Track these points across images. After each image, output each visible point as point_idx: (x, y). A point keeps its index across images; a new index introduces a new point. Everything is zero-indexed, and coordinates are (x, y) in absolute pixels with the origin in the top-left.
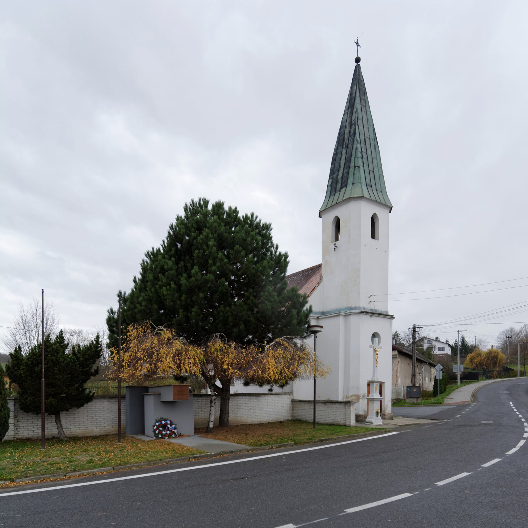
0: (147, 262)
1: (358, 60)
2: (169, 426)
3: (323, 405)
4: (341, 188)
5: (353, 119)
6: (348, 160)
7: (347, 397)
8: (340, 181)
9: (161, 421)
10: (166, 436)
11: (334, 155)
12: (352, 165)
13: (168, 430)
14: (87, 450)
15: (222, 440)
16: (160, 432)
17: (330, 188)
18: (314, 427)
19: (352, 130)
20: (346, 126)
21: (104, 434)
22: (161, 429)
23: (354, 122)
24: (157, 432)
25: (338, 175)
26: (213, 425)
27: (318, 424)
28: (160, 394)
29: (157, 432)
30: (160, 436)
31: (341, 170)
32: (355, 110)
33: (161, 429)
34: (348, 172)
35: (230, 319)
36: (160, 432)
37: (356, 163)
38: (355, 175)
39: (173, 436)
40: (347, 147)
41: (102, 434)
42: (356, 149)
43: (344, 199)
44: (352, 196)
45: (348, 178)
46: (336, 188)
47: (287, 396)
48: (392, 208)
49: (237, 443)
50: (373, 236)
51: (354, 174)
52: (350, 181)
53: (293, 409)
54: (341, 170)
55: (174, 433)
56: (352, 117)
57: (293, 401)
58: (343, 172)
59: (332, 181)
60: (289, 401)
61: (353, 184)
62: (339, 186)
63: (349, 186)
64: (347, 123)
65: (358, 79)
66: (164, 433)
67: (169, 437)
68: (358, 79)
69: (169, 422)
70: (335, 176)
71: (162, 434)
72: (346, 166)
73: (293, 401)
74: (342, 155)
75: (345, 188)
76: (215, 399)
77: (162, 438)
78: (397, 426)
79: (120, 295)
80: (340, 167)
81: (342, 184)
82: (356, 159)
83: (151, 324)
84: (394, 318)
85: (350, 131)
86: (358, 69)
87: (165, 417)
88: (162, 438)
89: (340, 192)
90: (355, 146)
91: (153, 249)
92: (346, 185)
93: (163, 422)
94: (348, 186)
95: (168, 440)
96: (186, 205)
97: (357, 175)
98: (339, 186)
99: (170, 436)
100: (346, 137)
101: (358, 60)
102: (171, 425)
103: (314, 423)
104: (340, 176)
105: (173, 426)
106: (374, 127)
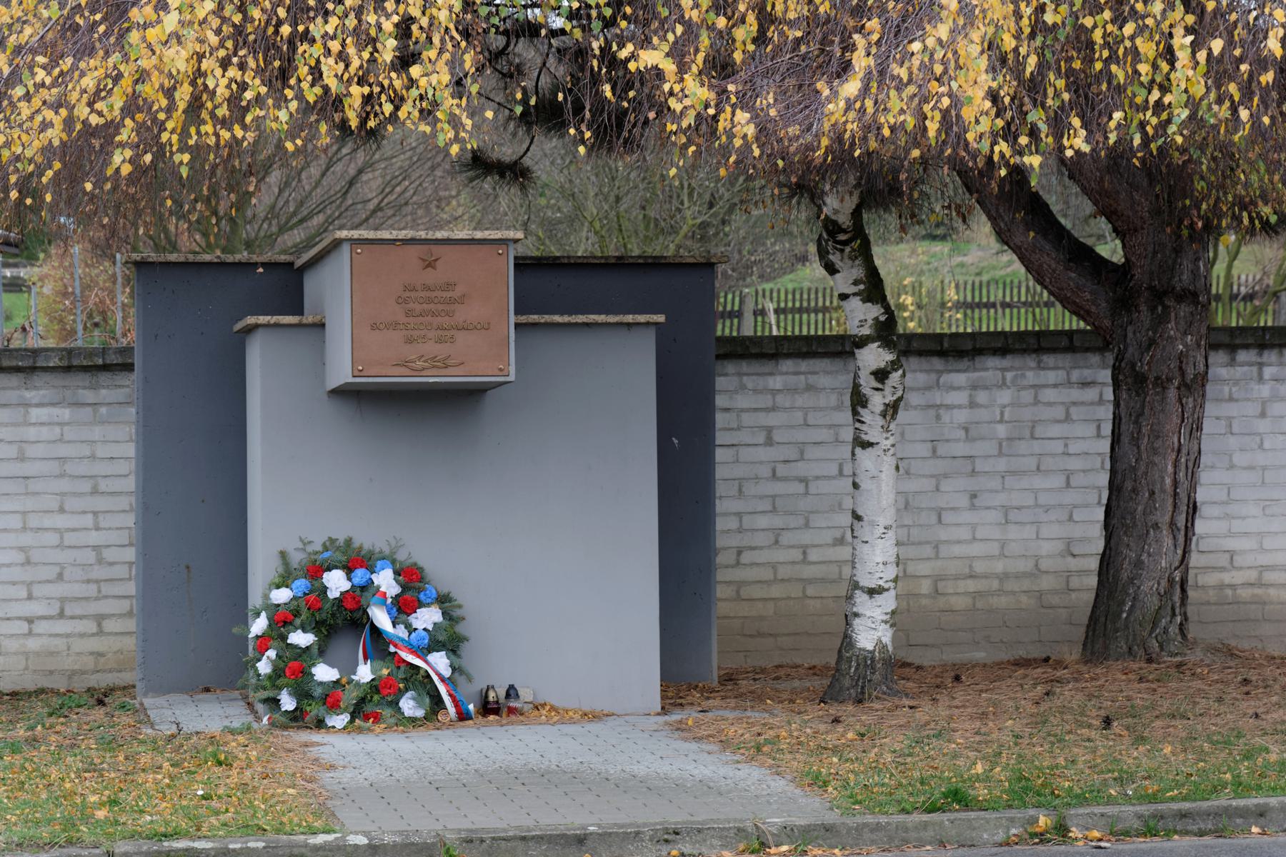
2: (381, 618)
9: (315, 571)
10: (334, 707)
13: (379, 644)
14: (296, 660)
22: (301, 638)
26: (894, 619)
33: (301, 638)
39: (409, 705)
55: (420, 681)
66: (324, 673)
67: (358, 711)
69: (386, 581)
76: (881, 375)
77: (296, 718)
84: (330, 539)
87: (366, 539)
88: (296, 718)
93: (336, 582)
99: (368, 708)
102: (403, 607)
105: (427, 618)
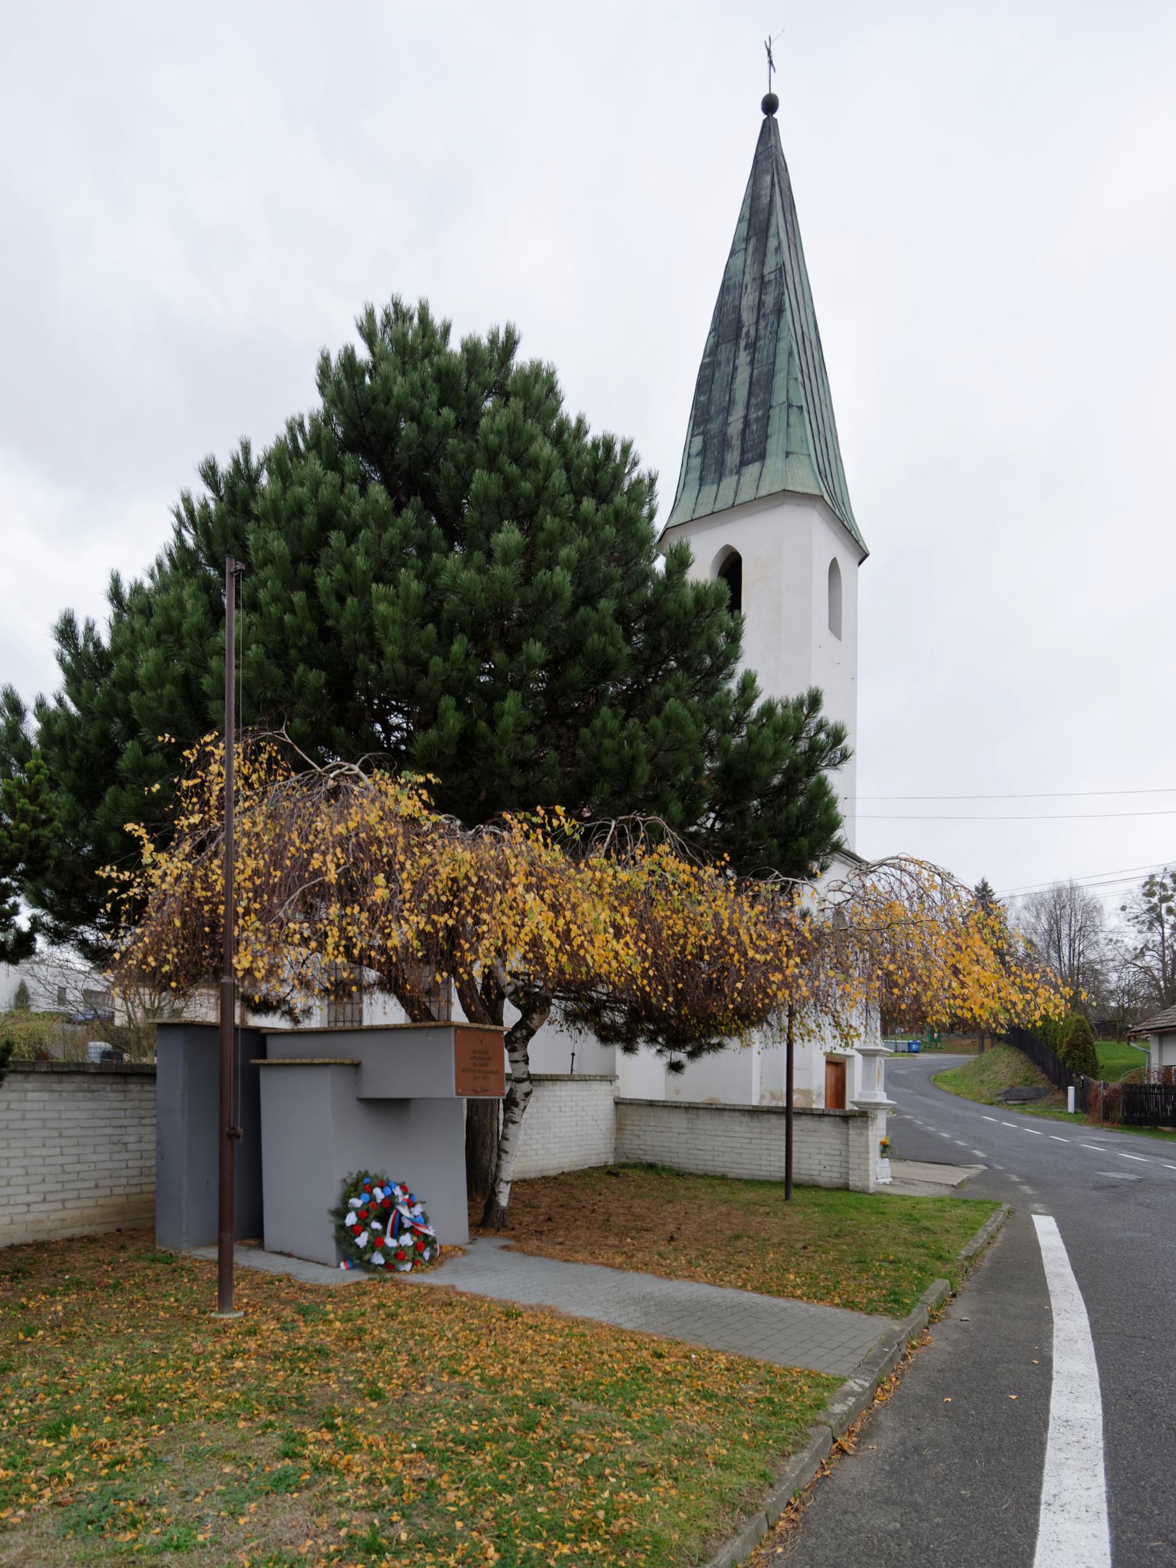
0: (205, 506)
1: (770, 105)
3: (746, 1119)
4: (743, 463)
5: (770, 265)
6: (762, 385)
7: (677, 1092)
8: (736, 443)
11: (703, 367)
12: (779, 397)
15: (670, 1275)
16: (376, 1243)
17: (696, 462)
18: (787, 1197)
19: (769, 300)
20: (741, 286)
21: (29, 1238)
23: (772, 276)
24: (362, 1240)
25: (726, 423)
27: (798, 1186)
28: (357, 1066)
29: (362, 1240)
30: (378, 1259)
31: (738, 413)
32: (772, 243)
34: (766, 420)
35: (644, 771)
36: (376, 1243)
37: (791, 395)
38: (792, 430)
40: (752, 347)
41: (17, 1240)
42: (791, 354)
43: (762, 492)
44: (790, 488)
45: (766, 436)
46: (721, 463)
47: (604, 1087)
48: (867, 556)
49: (756, 1289)
50: (835, 625)
51: (788, 425)
52: (775, 445)
53: (620, 1127)
54: (738, 413)
56: (762, 264)
57: (619, 1103)
58: (746, 418)
59: (705, 442)
60: (609, 1104)
61: (788, 454)
62: (733, 458)
63: (774, 461)
64: (748, 278)
65: (768, 159)
68: (768, 159)
70: (713, 427)
71: (385, 1251)
72: (754, 401)
73: (619, 1103)
74: (735, 368)
75: (757, 465)
78: (946, 1192)
79: (66, 631)
80: (732, 401)
81: (743, 452)
82: (791, 382)
83: (284, 748)
85: (761, 304)
86: (769, 132)
88: (389, 1267)
89: (739, 473)
90: (783, 346)
91: (246, 449)
92: (762, 457)
93: (379, 1194)
94: (769, 461)
95: (415, 1278)
96: (370, 315)
97: (796, 431)
98: (733, 458)
100: (748, 317)
101: (770, 105)
102: (411, 1204)
103: (788, 1183)
104: (735, 428)
105: (418, 1210)
106: (814, 313)
